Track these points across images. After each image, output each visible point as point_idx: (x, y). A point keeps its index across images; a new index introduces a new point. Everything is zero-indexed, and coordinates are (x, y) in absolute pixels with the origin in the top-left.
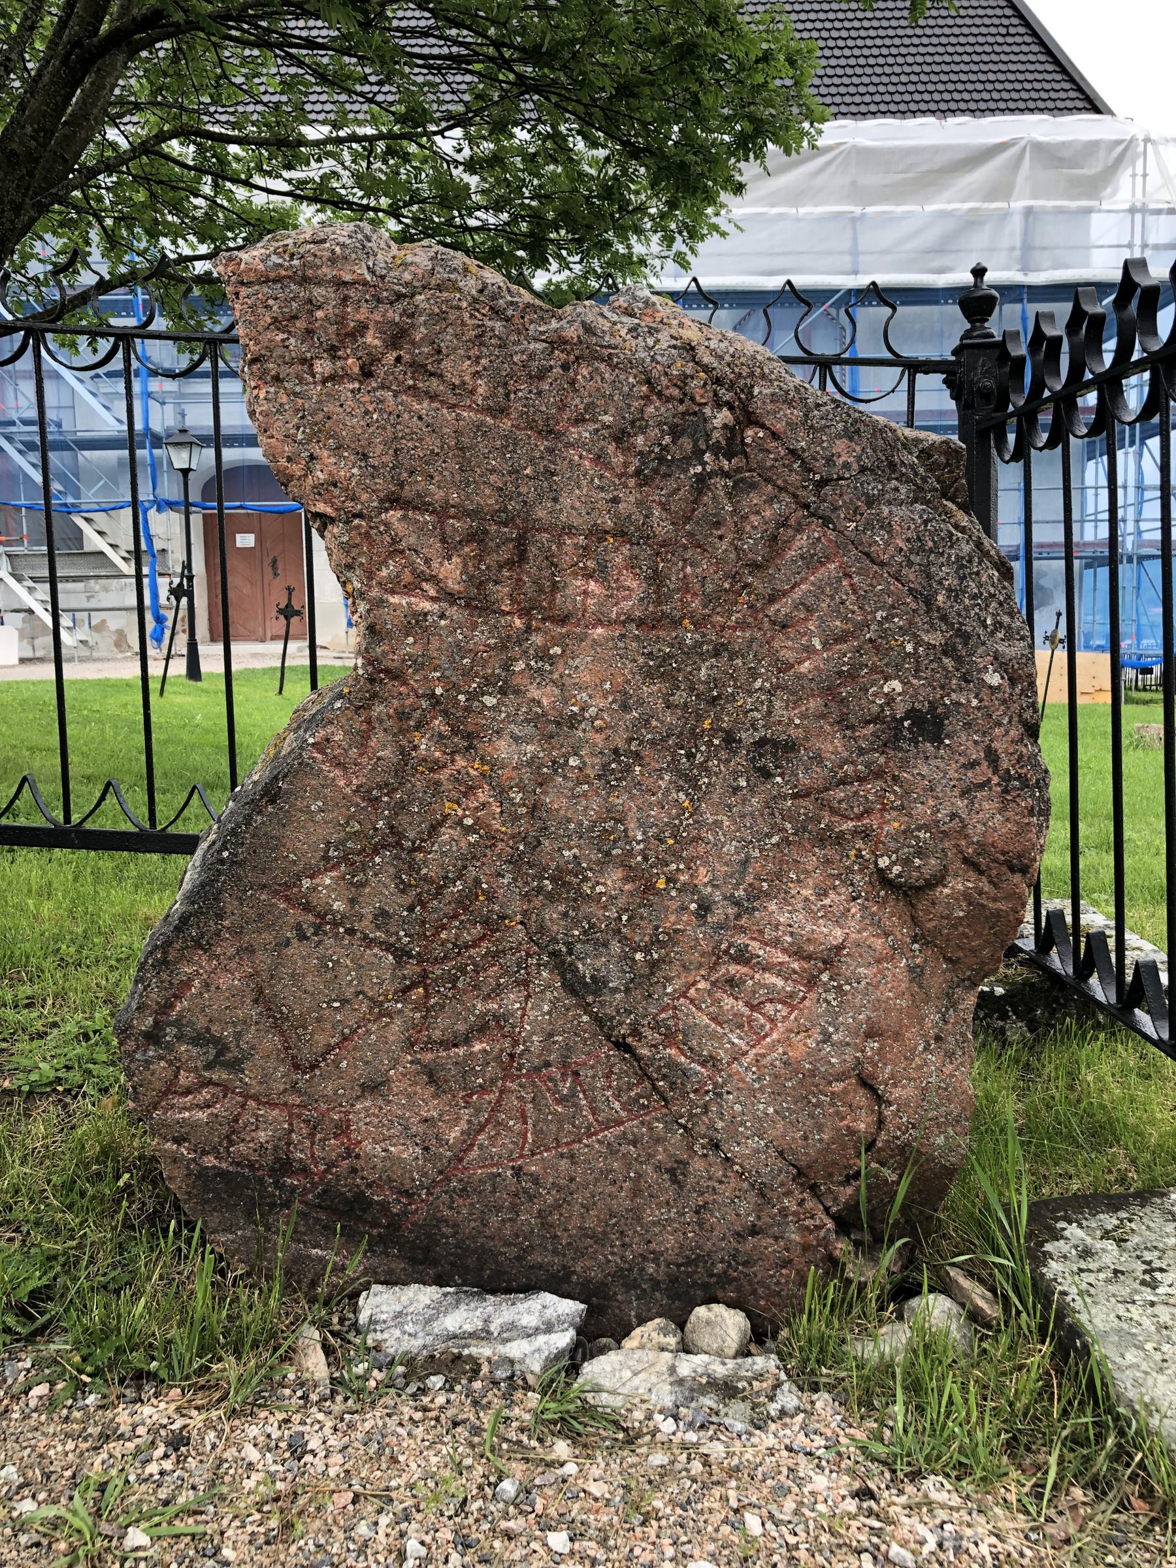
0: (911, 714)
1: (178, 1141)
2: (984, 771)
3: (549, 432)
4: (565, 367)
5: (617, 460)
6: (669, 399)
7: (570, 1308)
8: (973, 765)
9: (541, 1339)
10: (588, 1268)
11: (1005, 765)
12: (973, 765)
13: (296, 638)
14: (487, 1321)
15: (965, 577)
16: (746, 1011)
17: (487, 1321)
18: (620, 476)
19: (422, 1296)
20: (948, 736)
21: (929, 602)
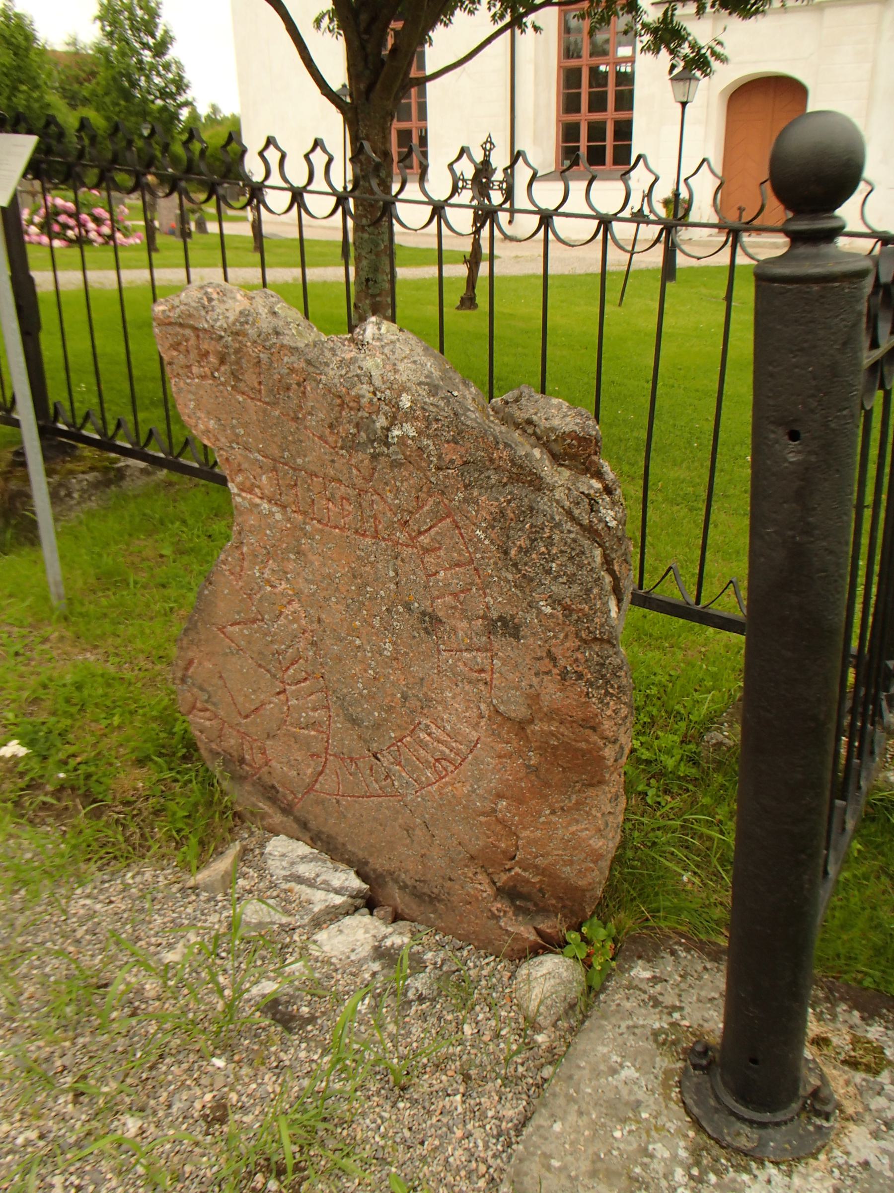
0: (501, 618)
1: (201, 732)
2: (547, 664)
3: (296, 419)
4: (299, 384)
5: (331, 439)
6: (351, 409)
7: (356, 883)
8: (540, 659)
9: (332, 895)
10: (378, 863)
11: (562, 662)
12: (540, 659)
13: (618, 273)
14: (318, 876)
15: (536, 539)
16: (433, 761)
17: (318, 876)
18: (334, 448)
19: (302, 849)
20: (523, 637)
21: (506, 553)
